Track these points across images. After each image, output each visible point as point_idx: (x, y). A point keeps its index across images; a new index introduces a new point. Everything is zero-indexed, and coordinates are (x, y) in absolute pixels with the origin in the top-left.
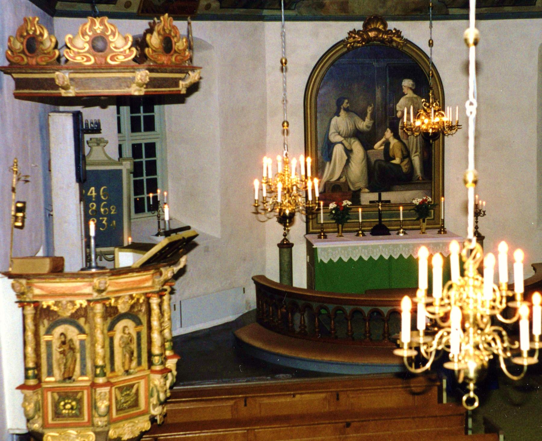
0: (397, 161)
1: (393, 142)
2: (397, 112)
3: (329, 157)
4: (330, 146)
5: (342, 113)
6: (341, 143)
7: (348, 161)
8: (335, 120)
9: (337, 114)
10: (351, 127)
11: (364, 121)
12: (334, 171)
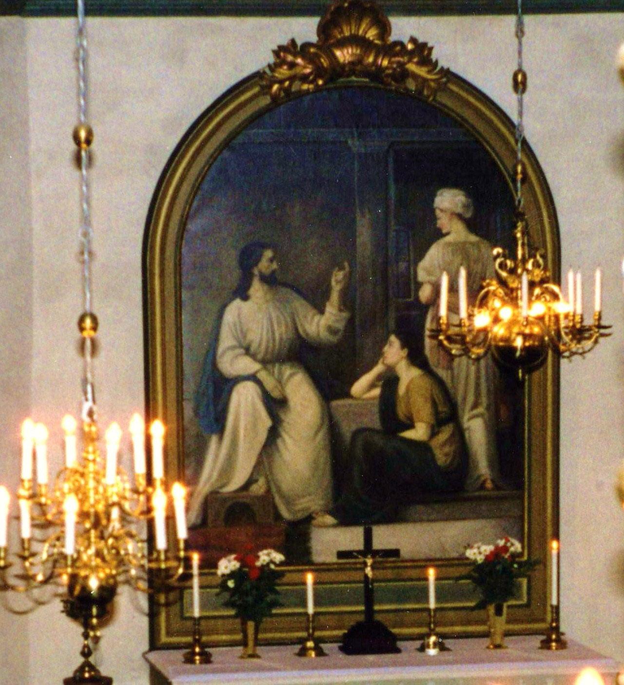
0: (419, 433)
1: (409, 375)
2: (419, 285)
3: (218, 423)
4: (220, 387)
5: (257, 289)
7: (274, 434)
8: (235, 310)
9: (242, 293)
10: (282, 332)
11: (322, 312)
12: (230, 459)
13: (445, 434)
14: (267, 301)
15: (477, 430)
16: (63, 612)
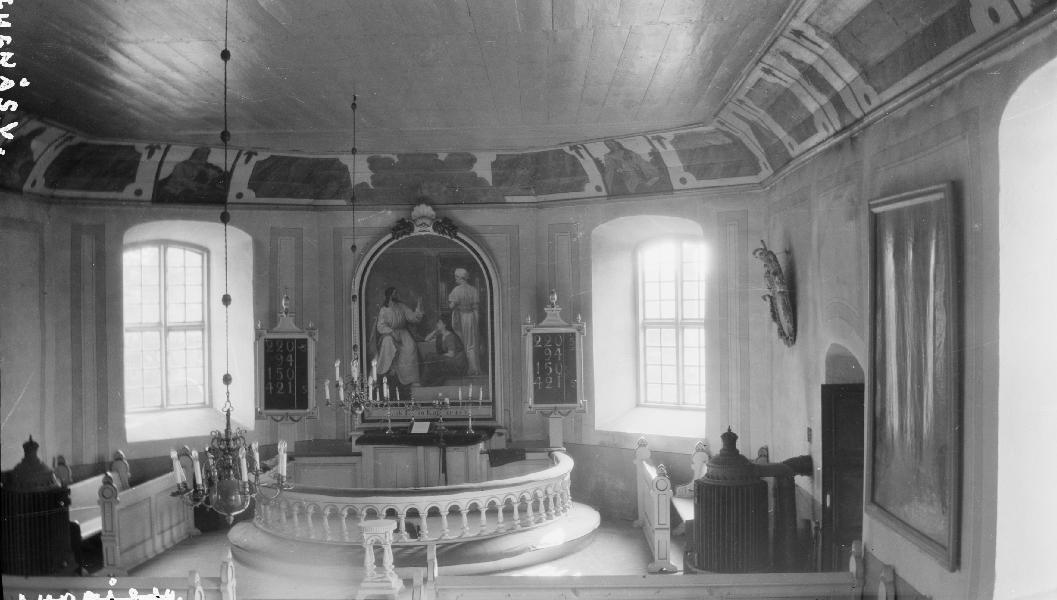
1: (446, 334)
2: (450, 302)
4: (379, 337)
6: (390, 334)
7: (398, 353)
10: (400, 318)
11: (414, 310)
13: (461, 354)
14: (111, 35)
15: (471, 353)
16: (729, 430)
